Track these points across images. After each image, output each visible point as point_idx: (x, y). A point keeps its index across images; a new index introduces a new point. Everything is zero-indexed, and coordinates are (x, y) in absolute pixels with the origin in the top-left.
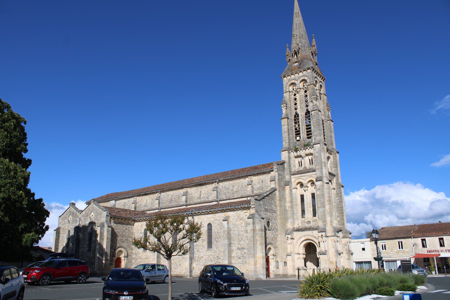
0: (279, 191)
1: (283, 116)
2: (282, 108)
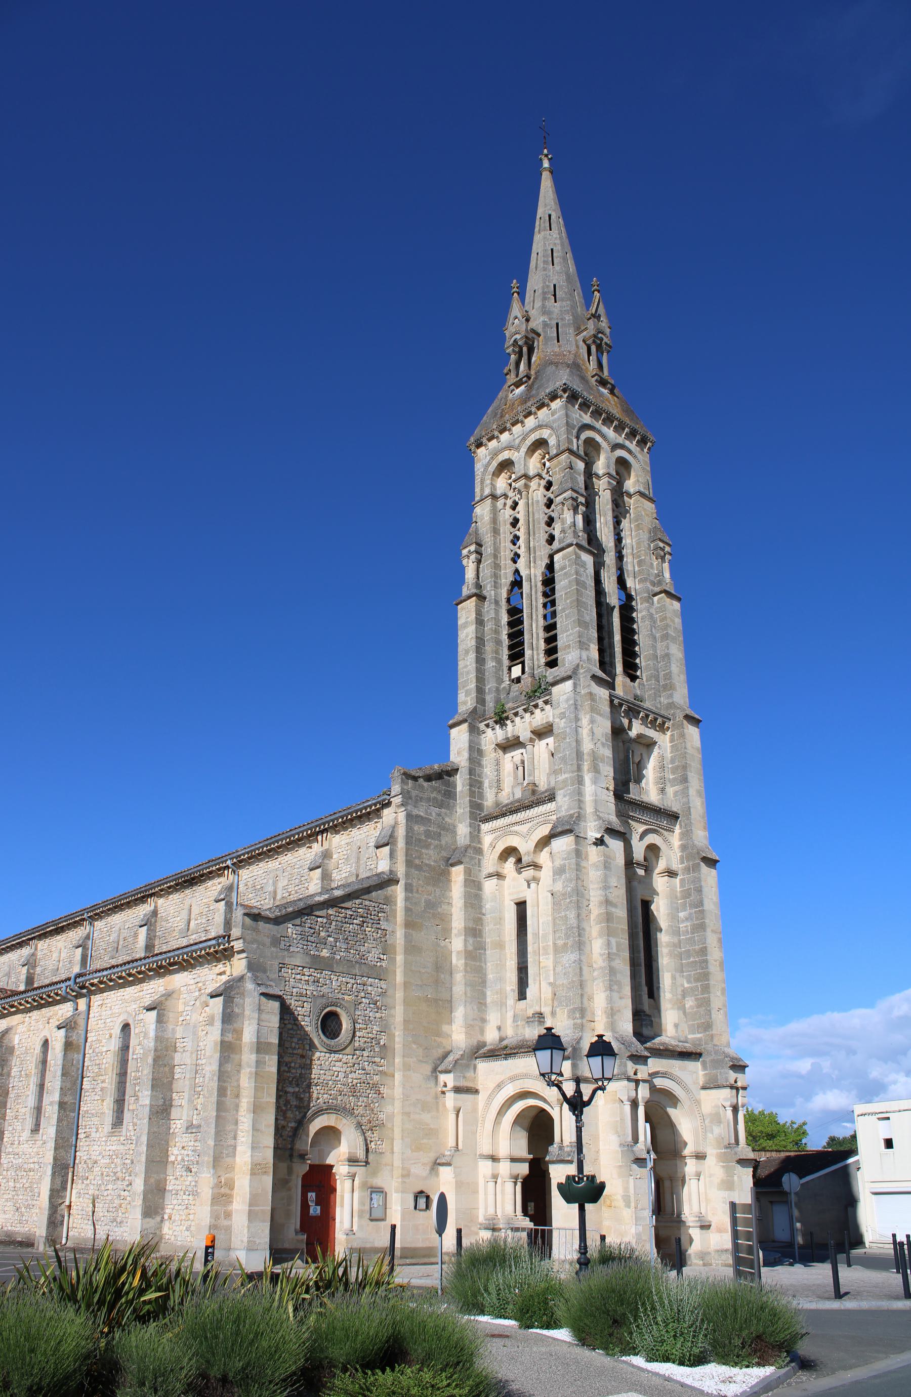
0: (408, 888)
1: (465, 592)
2: (465, 562)
